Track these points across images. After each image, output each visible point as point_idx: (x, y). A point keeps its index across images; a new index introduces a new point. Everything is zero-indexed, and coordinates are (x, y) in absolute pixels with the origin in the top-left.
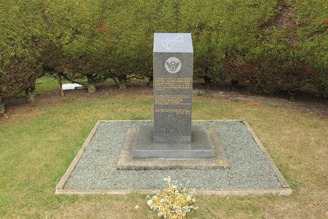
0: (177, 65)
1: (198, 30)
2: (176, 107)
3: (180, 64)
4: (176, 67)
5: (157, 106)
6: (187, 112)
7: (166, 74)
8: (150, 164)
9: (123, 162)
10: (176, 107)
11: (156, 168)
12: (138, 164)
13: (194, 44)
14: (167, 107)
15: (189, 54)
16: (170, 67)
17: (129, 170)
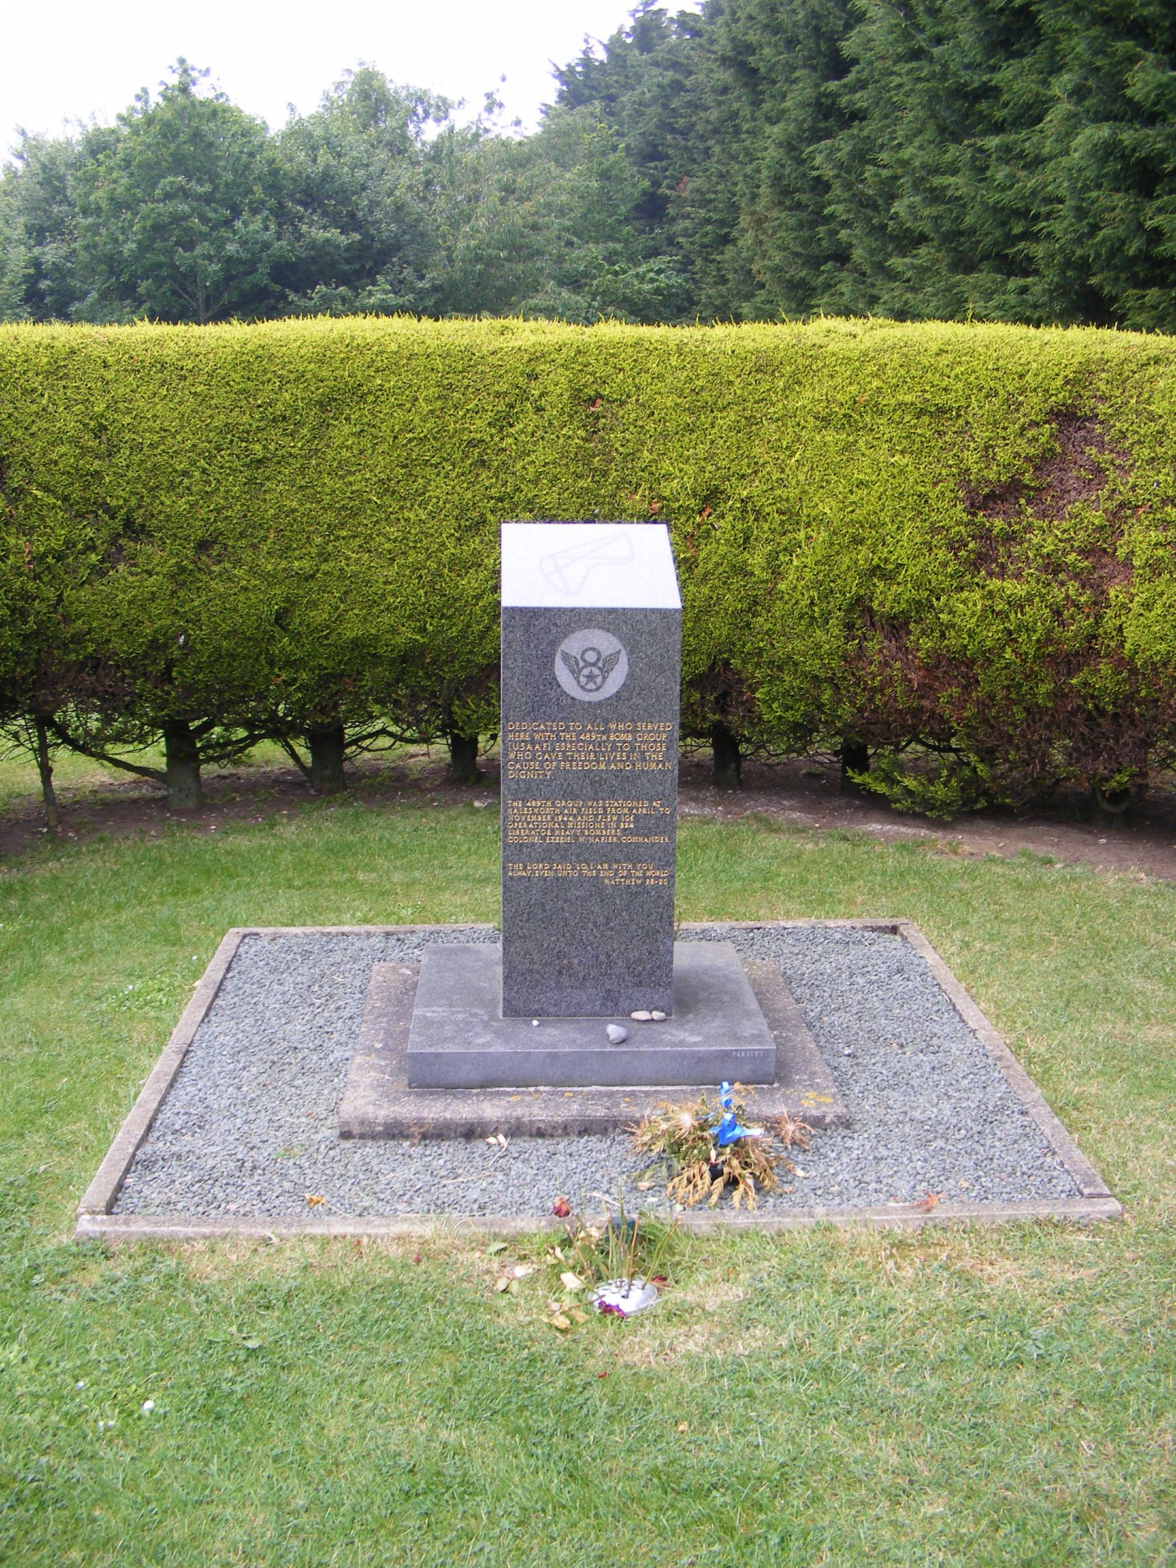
0: (607, 664)
1: (690, 516)
2: (606, 854)
3: (624, 658)
4: (606, 671)
5: (515, 852)
6: (655, 876)
7: (567, 708)
8: (490, 1109)
9: (365, 1094)
10: (606, 854)
11: (515, 1130)
12: (437, 1110)
13: (683, 586)
14: (561, 853)
15: (664, 614)
16: (575, 672)
17: (393, 1137)
